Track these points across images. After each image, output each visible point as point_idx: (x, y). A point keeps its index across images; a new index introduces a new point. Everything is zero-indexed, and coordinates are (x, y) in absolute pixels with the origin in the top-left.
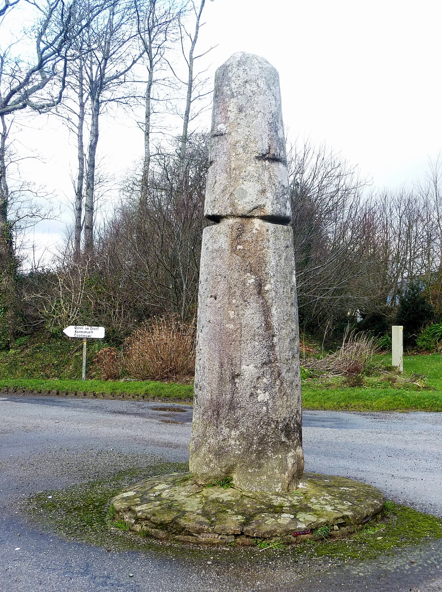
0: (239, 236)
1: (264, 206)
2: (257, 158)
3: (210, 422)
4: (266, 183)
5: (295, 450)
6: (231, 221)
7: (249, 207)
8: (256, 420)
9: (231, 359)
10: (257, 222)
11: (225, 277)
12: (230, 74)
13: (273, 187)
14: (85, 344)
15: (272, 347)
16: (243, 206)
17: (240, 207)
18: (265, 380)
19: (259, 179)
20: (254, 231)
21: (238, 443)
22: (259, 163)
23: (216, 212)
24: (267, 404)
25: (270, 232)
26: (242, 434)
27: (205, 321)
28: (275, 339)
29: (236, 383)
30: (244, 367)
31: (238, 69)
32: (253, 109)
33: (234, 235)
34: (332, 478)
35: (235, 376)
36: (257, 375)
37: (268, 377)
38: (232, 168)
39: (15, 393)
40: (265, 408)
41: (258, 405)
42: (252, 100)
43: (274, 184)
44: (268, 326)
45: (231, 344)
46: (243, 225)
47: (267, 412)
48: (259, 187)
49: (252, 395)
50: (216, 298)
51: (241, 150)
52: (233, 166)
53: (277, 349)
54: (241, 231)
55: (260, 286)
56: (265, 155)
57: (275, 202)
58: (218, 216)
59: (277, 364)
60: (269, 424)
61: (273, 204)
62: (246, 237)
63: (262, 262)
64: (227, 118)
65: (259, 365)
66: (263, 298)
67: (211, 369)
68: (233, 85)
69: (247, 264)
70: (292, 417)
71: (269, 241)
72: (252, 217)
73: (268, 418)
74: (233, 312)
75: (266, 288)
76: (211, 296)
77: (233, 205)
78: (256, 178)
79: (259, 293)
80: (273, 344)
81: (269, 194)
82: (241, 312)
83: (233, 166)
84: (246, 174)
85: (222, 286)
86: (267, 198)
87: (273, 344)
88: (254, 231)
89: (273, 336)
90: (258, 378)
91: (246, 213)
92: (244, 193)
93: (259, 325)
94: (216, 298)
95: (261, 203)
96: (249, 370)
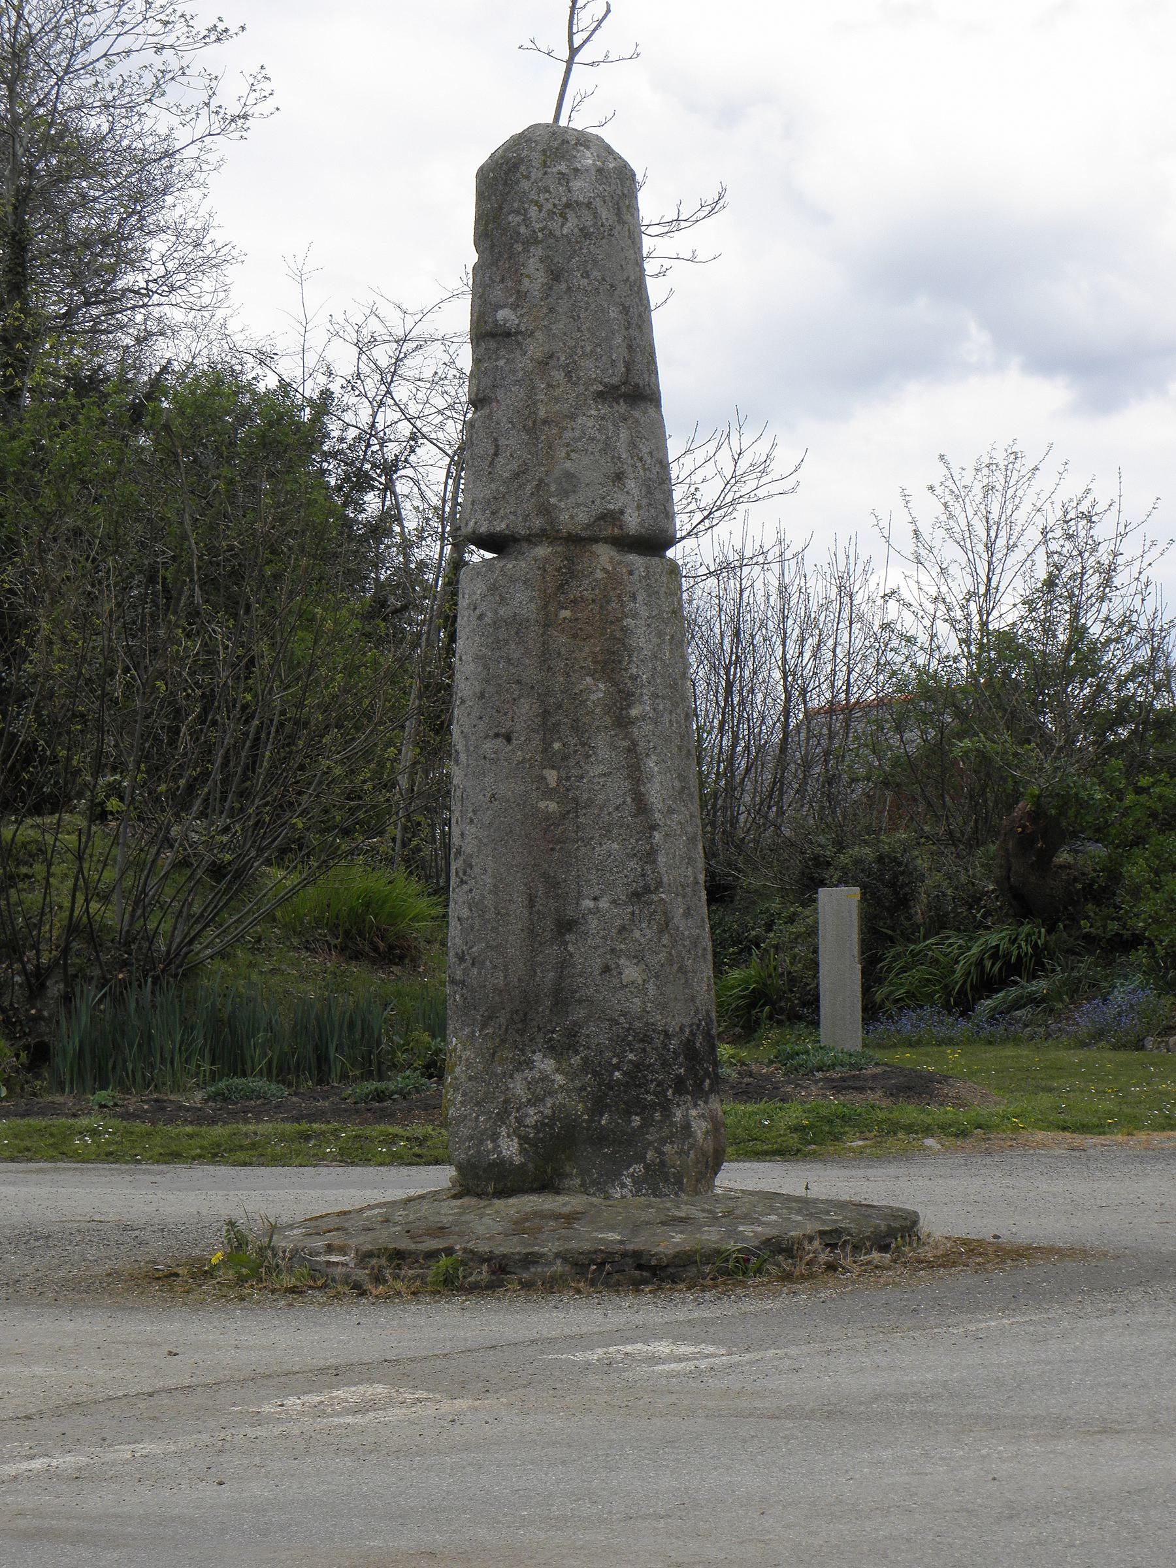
0: (562, 585)
1: (622, 512)
2: (600, 395)
3: (503, 1041)
4: (624, 456)
5: (706, 1102)
6: (542, 551)
7: (583, 517)
9: (553, 884)
10: (605, 555)
11: (532, 687)
12: (525, 185)
13: (639, 465)
15: (650, 856)
16: (574, 514)
17: (564, 517)
19: (607, 446)
20: (599, 575)
23: (500, 527)
25: (636, 576)
27: (481, 797)
28: (657, 836)
29: (567, 943)
31: (546, 173)
32: (586, 275)
34: (317, 1160)
35: (566, 926)
38: (539, 421)
39: (21, 1153)
42: (584, 251)
43: (641, 459)
44: (642, 806)
45: (552, 849)
49: (606, 969)
50: (509, 739)
51: (559, 376)
52: (542, 413)
53: (661, 859)
54: (569, 573)
56: (617, 388)
57: (645, 502)
58: (506, 536)
59: (663, 896)
61: (639, 507)
64: (521, 295)
67: (504, 911)
68: (533, 212)
70: (698, 1026)
72: (595, 540)
74: (554, 773)
75: (634, 712)
76: (497, 735)
77: (545, 510)
78: (601, 445)
80: (652, 848)
81: (631, 484)
83: (542, 413)
84: (577, 434)
85: (526, 708)
87: (652, 848)
88: (599, 575)
89: (653, 828)
91: (578, 530)
92: (570, 484)
94: (509, 739)
96: (600, 906)
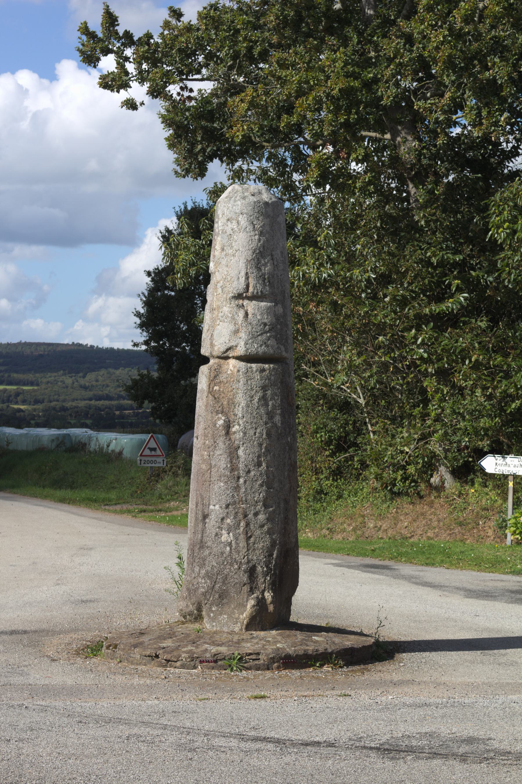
8: (221, 559)
14: (511, 484)
18: (229, 521)
21: (203, 581)
22: (234, 303)
24: (230, 544)
26: (207, 572)
30: (211, 507)
33: (212, 376)
36: (221, 516)
37: (232, 517)
40: (228, 549)
41: (222, 545)
46: (220, 366)
47: (231, 552)
48: (232, 327)
49: (217, 535)
55: (228, 427)
60: (231, 565)
62: (222, 377)
63: (232, 403)
65: (224, 506)
66: (230, 439)
69: (219, 405)
71: (239, 382)
73: (232, 558)
75: (234, 429)
79: (228, 433)
82: (212, 453)
84: (222, 314)
86: (240, 338)
90: (223, 519)
93: (225, 466)
95: (233, 344)
